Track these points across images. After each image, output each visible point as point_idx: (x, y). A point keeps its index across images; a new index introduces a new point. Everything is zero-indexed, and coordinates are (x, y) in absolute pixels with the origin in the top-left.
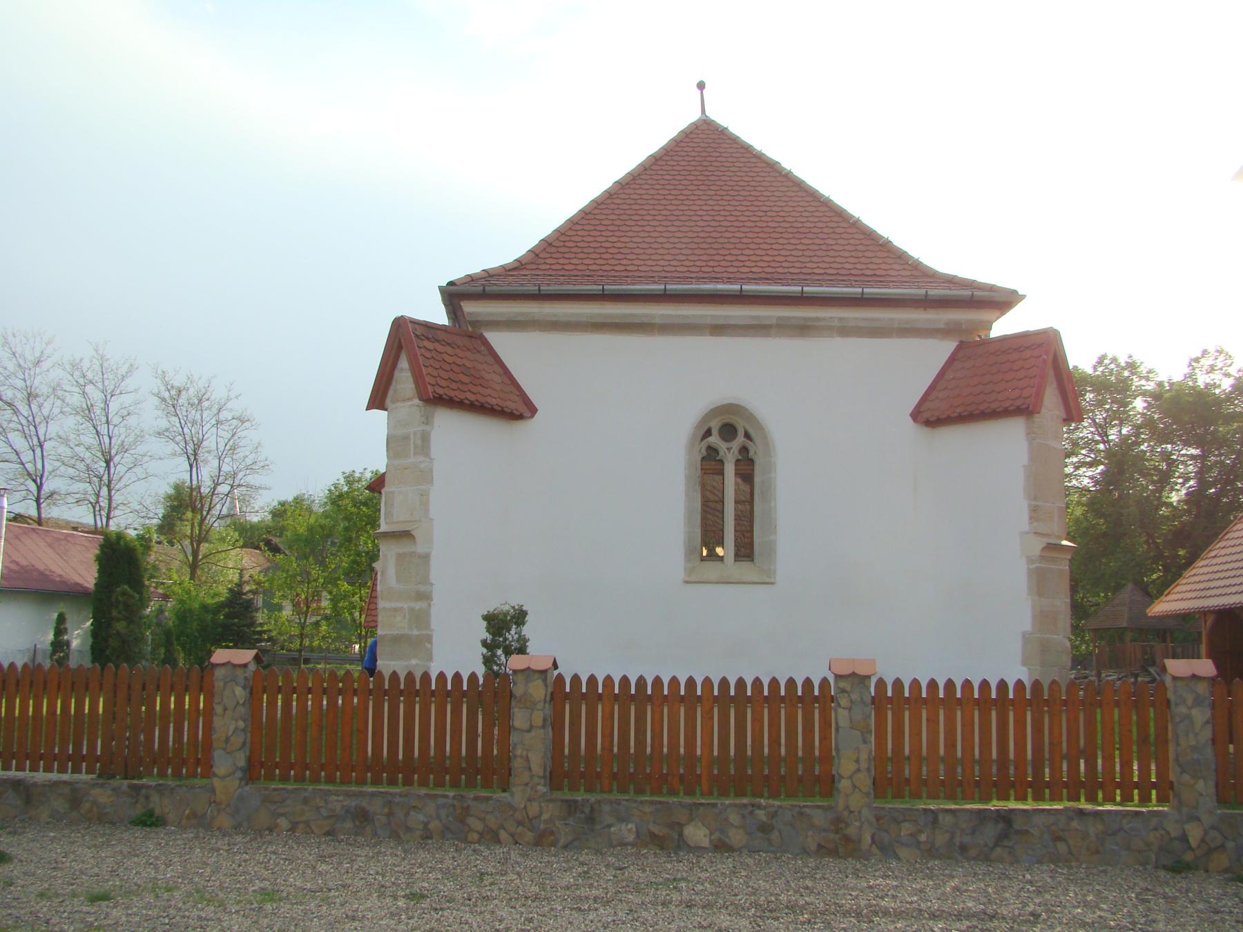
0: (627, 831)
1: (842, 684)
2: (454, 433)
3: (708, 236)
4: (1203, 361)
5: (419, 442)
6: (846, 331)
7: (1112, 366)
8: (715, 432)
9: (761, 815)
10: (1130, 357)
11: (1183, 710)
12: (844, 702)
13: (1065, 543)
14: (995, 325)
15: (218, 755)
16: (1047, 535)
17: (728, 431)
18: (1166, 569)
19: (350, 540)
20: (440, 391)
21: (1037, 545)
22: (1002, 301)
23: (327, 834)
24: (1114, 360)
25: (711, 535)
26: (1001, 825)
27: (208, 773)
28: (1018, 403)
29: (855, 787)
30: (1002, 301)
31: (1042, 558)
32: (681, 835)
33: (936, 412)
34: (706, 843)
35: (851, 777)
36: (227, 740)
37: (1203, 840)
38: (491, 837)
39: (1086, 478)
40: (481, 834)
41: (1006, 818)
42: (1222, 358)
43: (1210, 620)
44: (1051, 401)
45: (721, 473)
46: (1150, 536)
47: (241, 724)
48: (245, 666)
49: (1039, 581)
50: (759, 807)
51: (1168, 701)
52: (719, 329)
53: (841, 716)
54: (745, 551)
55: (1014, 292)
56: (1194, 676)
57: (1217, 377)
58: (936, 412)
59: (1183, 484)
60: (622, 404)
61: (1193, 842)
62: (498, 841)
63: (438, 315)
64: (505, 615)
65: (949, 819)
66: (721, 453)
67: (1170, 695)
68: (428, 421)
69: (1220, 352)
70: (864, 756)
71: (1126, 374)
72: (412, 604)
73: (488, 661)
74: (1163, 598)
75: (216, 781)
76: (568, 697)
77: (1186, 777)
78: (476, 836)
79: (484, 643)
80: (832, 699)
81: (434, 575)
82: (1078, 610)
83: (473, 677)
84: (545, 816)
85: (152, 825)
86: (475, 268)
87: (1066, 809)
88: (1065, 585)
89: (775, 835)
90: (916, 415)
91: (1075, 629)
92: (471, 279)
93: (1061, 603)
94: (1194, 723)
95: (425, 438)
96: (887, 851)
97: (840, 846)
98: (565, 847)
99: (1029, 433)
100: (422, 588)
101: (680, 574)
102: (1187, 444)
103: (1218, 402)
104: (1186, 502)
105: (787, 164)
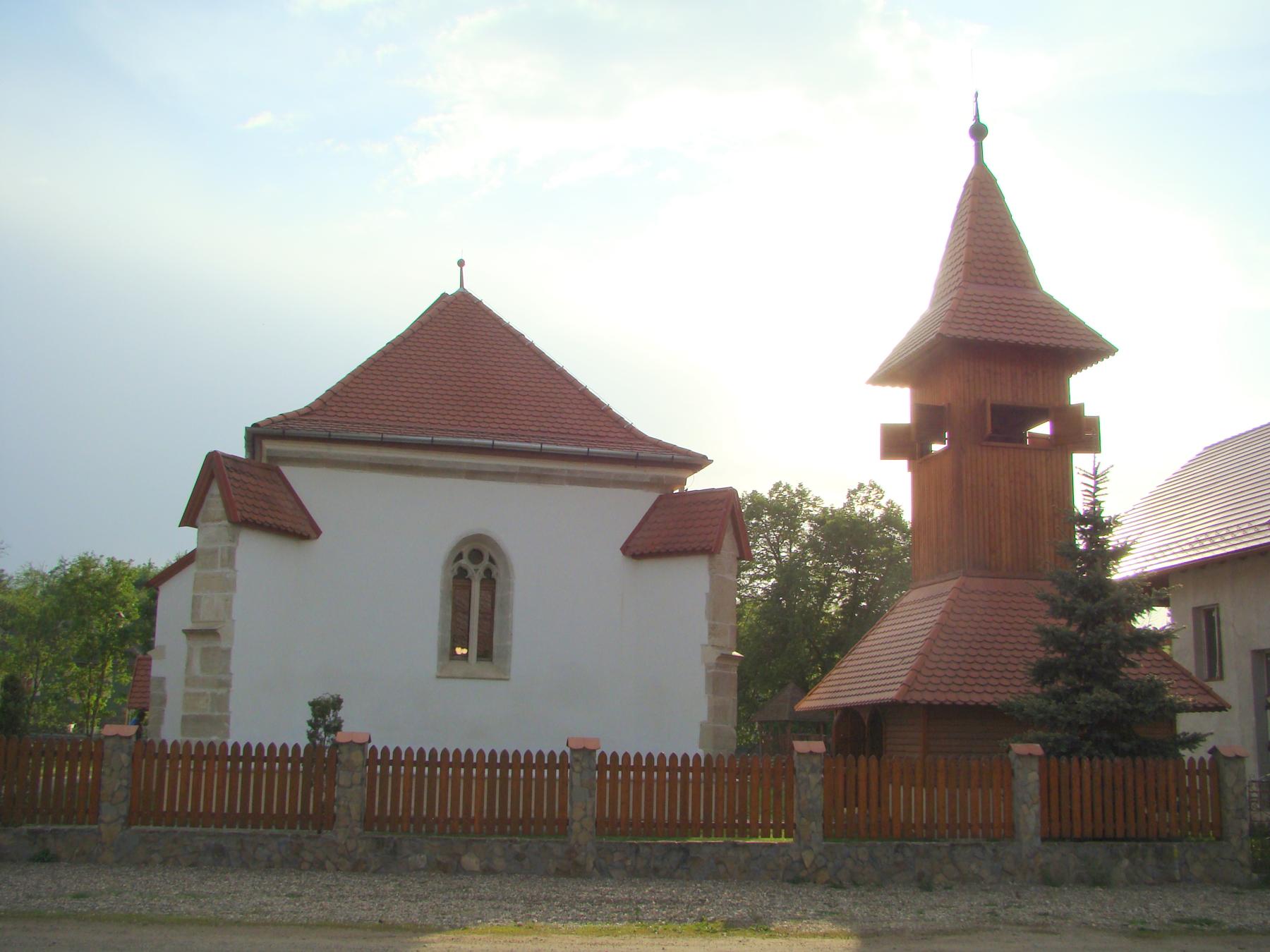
0: (421, 860)
1: (576, 756)
2: (256, 554)
3: (461, 390)
4: (859, 494)
6: (573, 480)
8: (465, 555)
9: (517, 847)
10: (800, 485)
11: (803, 775)
12: (577, 768)
13: (735, 653)
14: (689, 480)
15: (104, 806)
16: (722, 648)
17: (476, 556)
19: (84, 623)
20: (246, 515)
21: (713, 656)
22: (696, 462)
23: (193, 865)
24: (787, 487)
25: (459, 637)
26: (682, 854)
27: (96, 821)
29: (582, 828)
30: (696, 462)
31: (717, 665)
32: (459, 862)
33: (645, 546)
34: (477, 868)
35: (580, 821)
36: (113, 795)
37: (813, 862)
38: (319, 866)
41: (685, 849)
42: (874, 492)
44: (728, 542)
47: (125, 782)
48: (130, 737)
49: (715, 683)
50: (516, 842)
51: (794, 770)
52: (473, 474)
53: (575, 777)
54: (485, 653)
55: (705, 457)
58: (645, 546)
60: (390, 528)
61: (807, 864)
62: (325, 869)
63: (240, 451)
64: (327, 701)
65: (647, 849)
66: (470, 574)
67: (797, 766)
68: (234, 539)
69: (874, 486)
70: (589, 806)
72: (215, 690)
73: (311, 736)
74: (807, 698)
75: (103, 826)
76: (383, 764)
77: (804, 820)
78: (306, 865)
79: (310, 723)
80: (569, 766)
81: (233, 668)
83: (296, 747)
84: (360, 850)
86: (274, 413)
87: (725, 843)
88: (735, 685)
90: (625, 549)
92: (271, 421)
93: (731, 699)
95: (231, 554)
96: (603, 872)
97: (572, 869)
98: (375, 872)
99: (711, 568)
101: (433, 670)
102: (844, 564)
104: (842, 613)
105: (530, 335)
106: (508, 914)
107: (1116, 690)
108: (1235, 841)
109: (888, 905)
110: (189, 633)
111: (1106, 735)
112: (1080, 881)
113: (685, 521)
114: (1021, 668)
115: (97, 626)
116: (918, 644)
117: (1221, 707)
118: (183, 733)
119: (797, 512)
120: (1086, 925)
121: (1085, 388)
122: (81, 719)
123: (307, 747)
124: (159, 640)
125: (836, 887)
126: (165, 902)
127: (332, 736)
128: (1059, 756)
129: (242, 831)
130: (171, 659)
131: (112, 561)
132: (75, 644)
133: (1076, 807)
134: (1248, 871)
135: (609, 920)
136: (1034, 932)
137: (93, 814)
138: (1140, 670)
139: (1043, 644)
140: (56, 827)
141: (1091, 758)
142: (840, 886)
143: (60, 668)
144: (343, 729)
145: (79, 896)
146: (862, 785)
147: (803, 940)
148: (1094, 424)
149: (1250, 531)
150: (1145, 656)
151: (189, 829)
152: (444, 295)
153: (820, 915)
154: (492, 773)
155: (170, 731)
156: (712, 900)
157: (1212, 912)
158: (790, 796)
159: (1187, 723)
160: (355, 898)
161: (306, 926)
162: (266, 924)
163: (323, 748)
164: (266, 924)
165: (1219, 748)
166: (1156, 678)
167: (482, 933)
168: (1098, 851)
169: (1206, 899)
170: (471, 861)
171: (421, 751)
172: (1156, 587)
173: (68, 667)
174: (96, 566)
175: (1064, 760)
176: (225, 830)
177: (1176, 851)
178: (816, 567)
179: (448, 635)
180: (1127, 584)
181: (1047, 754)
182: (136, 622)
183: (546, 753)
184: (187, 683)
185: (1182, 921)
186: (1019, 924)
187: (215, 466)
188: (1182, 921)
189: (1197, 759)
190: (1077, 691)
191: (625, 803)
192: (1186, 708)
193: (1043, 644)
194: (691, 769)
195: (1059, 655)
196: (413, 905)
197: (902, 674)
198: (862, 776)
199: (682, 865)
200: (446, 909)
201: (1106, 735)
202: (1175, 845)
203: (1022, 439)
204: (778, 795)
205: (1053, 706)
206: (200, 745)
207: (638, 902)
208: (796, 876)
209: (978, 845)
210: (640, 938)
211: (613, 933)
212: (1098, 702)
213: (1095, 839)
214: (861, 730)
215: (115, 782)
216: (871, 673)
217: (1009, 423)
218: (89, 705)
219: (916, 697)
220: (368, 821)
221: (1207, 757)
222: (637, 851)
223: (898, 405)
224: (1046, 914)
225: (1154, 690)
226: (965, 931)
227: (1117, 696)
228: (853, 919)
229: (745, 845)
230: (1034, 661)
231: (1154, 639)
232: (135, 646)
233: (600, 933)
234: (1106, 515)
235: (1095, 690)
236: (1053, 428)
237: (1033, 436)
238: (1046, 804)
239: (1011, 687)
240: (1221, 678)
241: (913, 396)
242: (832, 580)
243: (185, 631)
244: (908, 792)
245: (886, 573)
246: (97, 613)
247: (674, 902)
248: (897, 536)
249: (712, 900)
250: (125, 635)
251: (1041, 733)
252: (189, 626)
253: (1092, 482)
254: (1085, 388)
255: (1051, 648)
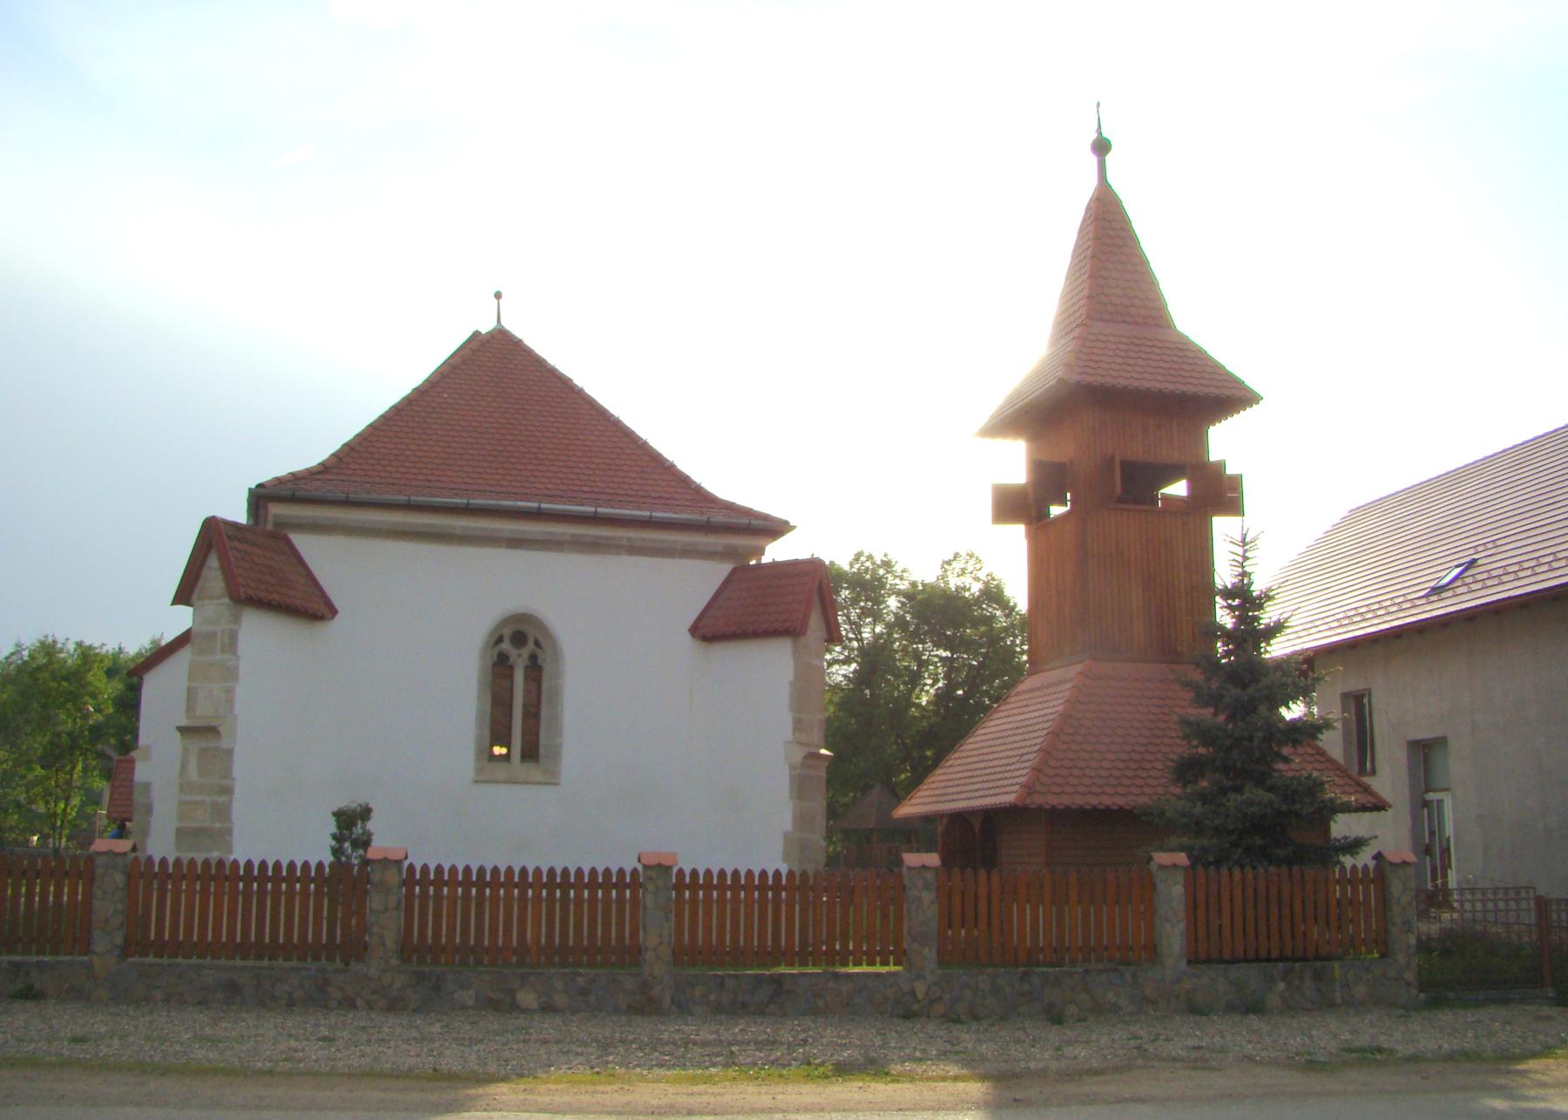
0: (467, 997)
1: (652, 874)
2: (261, 637)
3: (499, 446)
4: (954, 564)
5: (227, 640)
7: (868, 564)
8: (506, 639)
11: (915, 893)
12: (651, 887)
13: (823, 751)
15: (97, 934)
17: (519, 639)
18: (914, 769)
20: (251, 592)
21: (799, 754)
22: (775, 528)
23: (200, 1003)
24: (870, 557)
25: (500, 734)
27: (86, 947)
28: (787, 625)
30: (775, 528)
32: (513, 999)
33: (714, 628)
36: (106, 921)
38: (349, 1004)
39: (840, 673)
40: (340, 1002)
41: (778, 980)
42: (972, 561)
43: (945, 821)
45: (511, 677)
46: (898, 736)
48: (125, 854)
49: (800, 787)
50: (580, 975)
51: (904, 888)
52: (516, 543)
54: (531, 753)
55: (786, 523)
56: (924, 867)
57: (967, 580)
58: (714, 628)
59: (932, 686)
60: (419, 607)
61: (920, 996)
64: (354, 811)
67: (906, 882)
68: (236, 619)
71: (881, 572)
72: (215, 798)
73: (336, 852)
76: (424, 887)
78: (335, 1003)
79: (334, 837)
82: (832, 812)
85: (35, 998)
86: (282, 470)
89: (592, 999)
91: (830, 832)
92: (279, 481)
93: (818, 804)
94: (924, 908)
95: (233, 637)
96: (682, 1008)
97: (646, 1006)
98: (414, 1011)
99: (796, 653)
100: (224, 782)
102: (937, 645)
103: (968, 604)
105: (579, 380)
106: (580, 1059)
107: (1270, 789)
108: (1401, 959)
109: (1018, 1041)
110: (183, 730)
111: (1258, 841)
112: (1231, 1008)
113: (765, 598)
114: (1160, 766)
115: (65, 721)
116: (1038, 738)
117: (1380, 806)
118: (178, 846)
119: (883, 586)
120: (1249, 1058)
121: (1226, 442)
122: (46, 830)
123: (332, 865)
124: (143, 739)
125: (953, 1021)
126: (178, 1047)
127: (361, 852)
128: (1206, 866)
129: (258, 963)
130: (160, 758)
131: (79, 644)
132: (38, 743)
133: (1226, 921)
134: (1414, 992)
135: (699, 1065)
136: (1195, 1068)
137: (84, 944)
138: (1295, 765)
139: (1186, 737)
140: (41, 958)
141: (1242, 867)
142: (958, 1021)
143: (22, 771)
144: (373, 844)
145: (76, 1040)
146: (983, 904)
147: (934, 1084)
148: (1235, 483)
149: (1405, 606)
150: (1301, 750)
151: (195, 961)
152: (476, 334)
153: (944, 1055)
154: (551, 894)
155: (161, 844)
156: (815, 1040)
157: (1382, 1038)
158: (899, 918)
159: (1343, 826)
160: (399, 1041)
161: (350, 1075)
162: (301, 1074)
163: (349, 866)
164: (301, 1074)
165: (1385, 853)
166: (1315, 774)
167: (557, 1082)
168: (1251, 975)
169: (1371, 1024)
170: (527, 997)
171: (467, 869)
172: (1305, 671)
173: (31, 769)
174: (61, 651)
175: (1212, 869)
176: (238, 962)
177: (1337, 972)
178: (904, 649)
179: (487, 733)
180: (1281, 664)
181: (1193, 865)
182: (108, 717)
183: (600, 870)
184: (182, 789)
185: (1350, 1050)
186: (1174, 1060)
187: (213, 534)
188: (1350, 1050)
189: (1360, 867)
190: (1224, 791)
191: (708, 930)
192: (1347, 808)
193: (1186, 737)
194: (701, 887)
195: (1202, 750)
196: (468, 1050)
197: (1022, 775)
198: (983, 891)
199: (775, 1000)
200: (507, 1054)
201: (1258, 841)
202: (1336, 965)
203: (1154, 500)
204: (885, 917)
205: (1198, 809)
206: (206, 863)
207: (730, 1044)
208: (905, 1009)
209: (1115, 970)
210: (742, 1087)
211: (709, 1080)
212: (1251, 803)
213: (1246, 960)
214: (973, 838)
215: (108, 907)
216: (989, 768)
217: (1138, 482)
218: (55, 815)
219: (1038, 800)
220: (406, 950)
221: (1371, 864)
222: (722, 984)
223: (1012, 462)
224: (1199, 1048)
225: (1314, 787)
226: (1115, 1070)
227: (1271, 796)
228: (983, 1059)
229: (848, 975)
230: (1175, 757)
231: (1303, 732)
232: (109, 746)
233: (694, 1080)
234: (1257, 589)
235: (1247, 789)
236: (1191, 487)
237: (1166, 498)
238: (1192, 922)
239: (1152, 789)
240: (1373, 772)
241: (1030, 452)
242: (923, 664)
243: (180, 729)
244: (1035, 910)
245: (985, 656)
246: (66, 711)
247: (773, 1043)
248: (998, 613)
249: (815, 1040)
250: (97, 732)
251: (1185, 840)
252: (184, 722)
253: (1240, 551)
254: (1226, 442)
255: (1195, 742)
